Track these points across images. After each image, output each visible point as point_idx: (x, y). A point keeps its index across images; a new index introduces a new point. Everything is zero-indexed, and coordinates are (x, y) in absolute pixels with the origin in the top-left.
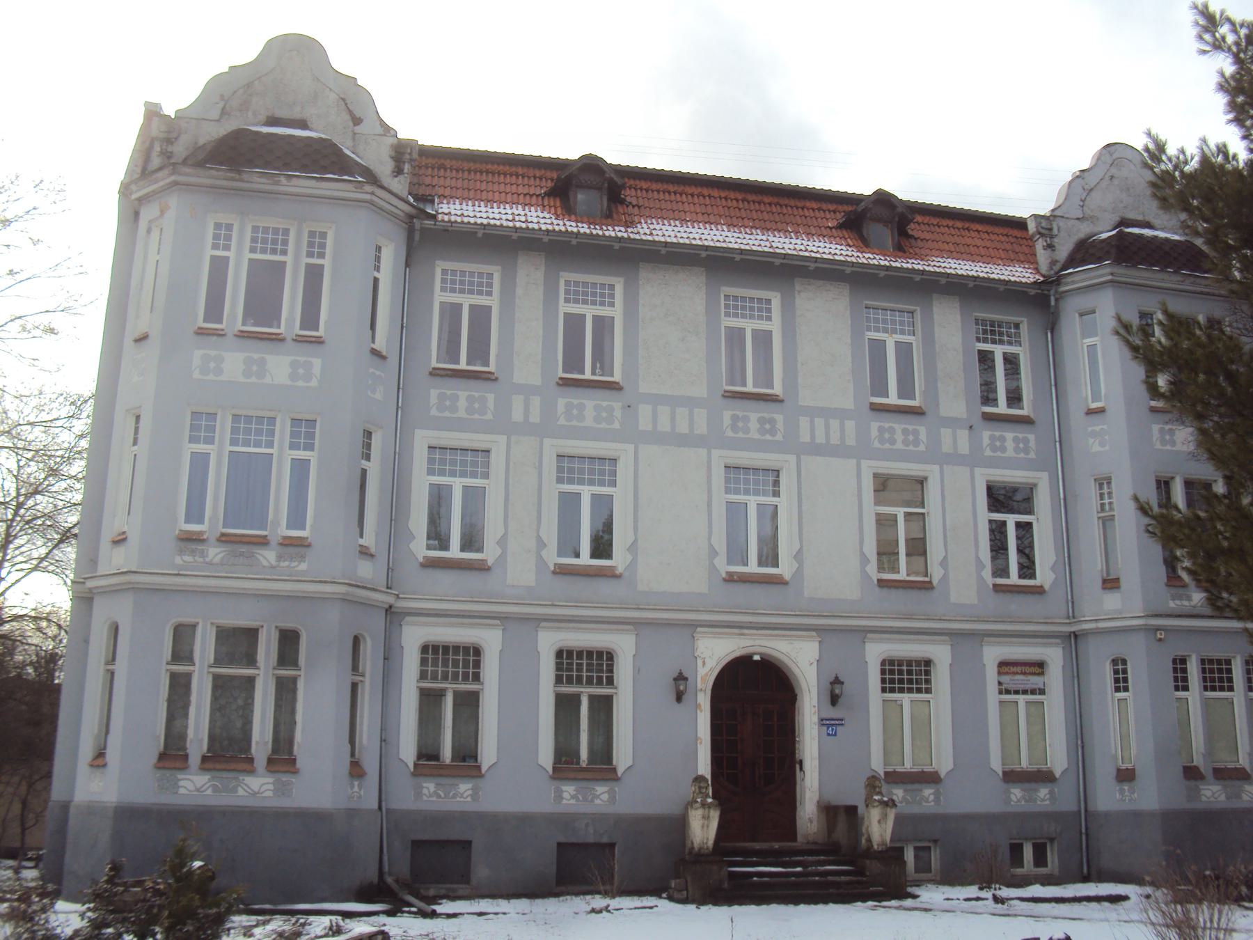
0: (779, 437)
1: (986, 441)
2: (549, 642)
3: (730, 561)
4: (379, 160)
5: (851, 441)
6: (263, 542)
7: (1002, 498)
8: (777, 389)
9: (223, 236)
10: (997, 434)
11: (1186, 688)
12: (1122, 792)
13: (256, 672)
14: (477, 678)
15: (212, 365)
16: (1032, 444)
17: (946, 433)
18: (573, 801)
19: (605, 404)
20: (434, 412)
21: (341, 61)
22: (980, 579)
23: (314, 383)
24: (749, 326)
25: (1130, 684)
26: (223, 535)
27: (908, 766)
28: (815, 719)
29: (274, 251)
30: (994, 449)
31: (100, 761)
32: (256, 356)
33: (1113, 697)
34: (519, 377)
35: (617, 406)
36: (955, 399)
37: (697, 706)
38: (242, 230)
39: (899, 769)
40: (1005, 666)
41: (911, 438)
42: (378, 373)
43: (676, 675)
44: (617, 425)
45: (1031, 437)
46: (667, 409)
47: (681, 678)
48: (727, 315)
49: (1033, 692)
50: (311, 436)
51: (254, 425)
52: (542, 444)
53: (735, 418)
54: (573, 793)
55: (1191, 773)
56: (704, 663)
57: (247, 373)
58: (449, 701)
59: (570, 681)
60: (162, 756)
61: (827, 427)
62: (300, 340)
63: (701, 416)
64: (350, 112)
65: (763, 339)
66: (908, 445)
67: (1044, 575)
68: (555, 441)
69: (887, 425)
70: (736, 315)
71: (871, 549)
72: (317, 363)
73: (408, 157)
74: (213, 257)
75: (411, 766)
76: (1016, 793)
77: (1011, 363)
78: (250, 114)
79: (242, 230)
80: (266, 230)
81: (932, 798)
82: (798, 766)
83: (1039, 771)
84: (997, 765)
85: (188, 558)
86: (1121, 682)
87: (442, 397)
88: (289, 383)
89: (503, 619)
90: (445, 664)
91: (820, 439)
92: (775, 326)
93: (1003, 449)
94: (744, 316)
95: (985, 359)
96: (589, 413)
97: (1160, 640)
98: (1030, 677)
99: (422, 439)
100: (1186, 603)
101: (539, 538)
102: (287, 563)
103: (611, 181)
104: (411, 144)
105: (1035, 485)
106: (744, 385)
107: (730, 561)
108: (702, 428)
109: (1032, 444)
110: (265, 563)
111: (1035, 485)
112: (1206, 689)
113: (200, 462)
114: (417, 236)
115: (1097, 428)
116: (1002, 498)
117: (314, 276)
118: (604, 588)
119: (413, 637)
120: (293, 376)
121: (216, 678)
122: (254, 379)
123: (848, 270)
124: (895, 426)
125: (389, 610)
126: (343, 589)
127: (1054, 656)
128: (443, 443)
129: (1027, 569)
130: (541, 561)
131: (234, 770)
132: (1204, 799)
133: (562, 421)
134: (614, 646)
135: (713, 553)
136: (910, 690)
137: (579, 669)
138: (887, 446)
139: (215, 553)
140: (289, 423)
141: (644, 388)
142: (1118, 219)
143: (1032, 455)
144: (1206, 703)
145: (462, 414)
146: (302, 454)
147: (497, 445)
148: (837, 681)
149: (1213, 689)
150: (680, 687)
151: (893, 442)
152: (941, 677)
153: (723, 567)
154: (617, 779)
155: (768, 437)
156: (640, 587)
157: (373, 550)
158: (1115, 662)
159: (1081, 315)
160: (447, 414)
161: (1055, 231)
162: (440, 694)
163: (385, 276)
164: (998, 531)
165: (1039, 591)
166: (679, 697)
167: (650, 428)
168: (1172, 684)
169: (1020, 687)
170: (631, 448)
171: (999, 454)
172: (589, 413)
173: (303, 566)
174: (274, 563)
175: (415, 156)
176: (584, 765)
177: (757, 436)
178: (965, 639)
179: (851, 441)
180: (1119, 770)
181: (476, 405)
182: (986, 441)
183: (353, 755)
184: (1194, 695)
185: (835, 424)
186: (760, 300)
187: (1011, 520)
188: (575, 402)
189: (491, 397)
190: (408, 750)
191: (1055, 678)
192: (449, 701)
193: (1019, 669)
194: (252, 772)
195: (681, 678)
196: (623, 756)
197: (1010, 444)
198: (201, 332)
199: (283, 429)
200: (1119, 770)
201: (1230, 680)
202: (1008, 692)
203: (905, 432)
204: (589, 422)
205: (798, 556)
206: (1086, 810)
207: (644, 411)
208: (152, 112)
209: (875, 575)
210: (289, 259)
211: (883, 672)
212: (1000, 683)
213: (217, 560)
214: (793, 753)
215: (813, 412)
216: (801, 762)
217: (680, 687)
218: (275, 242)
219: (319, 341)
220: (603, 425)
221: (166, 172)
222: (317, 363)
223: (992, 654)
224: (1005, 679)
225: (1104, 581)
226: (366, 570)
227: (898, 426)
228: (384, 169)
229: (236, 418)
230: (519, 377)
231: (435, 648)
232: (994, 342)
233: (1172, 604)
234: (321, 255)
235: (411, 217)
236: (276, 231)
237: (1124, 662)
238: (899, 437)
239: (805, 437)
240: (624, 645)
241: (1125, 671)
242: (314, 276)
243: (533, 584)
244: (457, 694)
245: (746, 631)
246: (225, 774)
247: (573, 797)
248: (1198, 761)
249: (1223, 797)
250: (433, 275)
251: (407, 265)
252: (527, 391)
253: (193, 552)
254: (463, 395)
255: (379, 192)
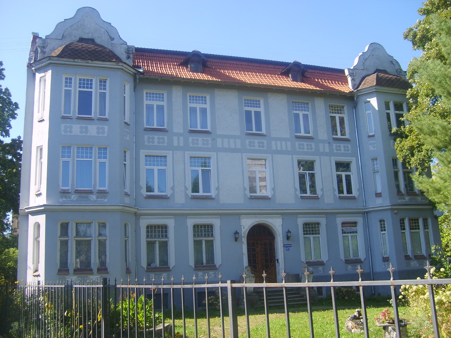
0: (265, 148)
1: (334, 147)
2: (191, 222)
3: (251, 192)
4: (121, 52)
5: (289, 149)
6: (91, 192)
7: (343, 166)
8: (209, 129)
9: (69, 81)
10: (338, 145)
11: (404, 229)
12: (385, 265)
13: (68, 238)
14: (166, 236)
15: (68, 129)
16: (350, 148)
17: (321, 145)
18: (202, 278)
19: (205, 138)
20: (146, 143)
21: (105, 17)
22: (334, 195)
23: (106, 135)
24: (198, 106)
25: (386, 228)
26: (76, 190)
27: (313, 260)
28: (282, 245)
29: (87, 88)
30: (337, 150)
31: (37, 274)
32: (84, 126)
33: (380, 233)
34: (175, 130)
35: (209, 139)
36: (323, 133)
37: (242, 242)
38: (76, 79)
39: (349, 258)
40: (344, 224)
41: (309, 147)
42: (127, 130)
43: (235, 232)
44: (210, 146)
45: (349, 146)
46: (176, 137)
47: (236, 233)
48: (190, 102)
49: (353, 232)
50: (105, 154)
51: (85, 149)
52: (330, 158)
53: (250, 142)
54: (202, 275)
55: (407, 257)
56: (244, 228)
57: (81, 132)
58: (157, 245)
59: (198, 236)
60: (59, 271)
61: (281, 144)
62: (99, 119)
63: (238, 142)
64: (110, 36)
65: (204, 111)
66: (308, 150)
67: (355, 193)
68: (189, 152)
69: (301, 143)
70: (248, 106)
71: (247, 186)
72: (106, 128)
73: (131, 52)
74: (79, 91)
75: (146, 269)
76: (350, 267)
77: (342, 121)
78: (73, 37)
79: (76, 79)
80: (84, 80)
81: (322, 270)
82: (276, 262)
83: (357, 259)
84: (342, 257)
85: (65, 199)
86: (383, 229)
87: (149, 138)
88: (97, 135)
89: (175, 215)
90: (155, 232)
91: (279, 148)
92: (207, 106)
93: (340, 150)
94: (153, 100)
95: (333, 118)
96: (200, 142)
97: (396, 213)
98: (352, 228)
99: (143, 153)
100: (403, 200)
101: (185, 186)
102: (100, 199)
103: (203, 59)
104: (132, 47)
105: (315, 161)
106: (153, 125)
107: (251, 192)
108: (239, 146)
109: (350, 148)
110: (92, 200)
111: (315, 161)
112: (411, 229)
113: (66, 164)
114: (138, 80)
115: (372, 142)
116: (343, 166)
117: (103, 96)
118: (209, 203)
119: (144, 223)
120: (98, 133)
121: (77, 241)
122: (84, 134)
123: (287, 90)
124: (304, 143)
125: (135, 214)
126: (120, 208)
127: (360, 220)
128: (194, 155)
129: (349, 191)
130: (186, 195)
131: (86, 274)
132: (412, 266)
133: (191, 145)
134: (213, 223)
135: (186, 189)
136: (313, 234)
137: (201, 232)
138: (302, 150)
139: (74, 197)
140: (97, 149)
141: (219, 132)
142: (375, 69)
143: (350, 152)
144: (411, 233)
145: (156, 144)
146: (102, 160)
147: (169, 154)
148: (289, 232)
149: (413, 229)
150: (236, 236)
151: (303, 149)
152: (323, 229)
153: (249, 194)
154: (217, 269)
155: (262, 148)
156: (221, 202)
157: (129, 193)
158: (380, 221)
159: (365, 103)
160: (151, 144)
161: (355, 74)
162: (154, 243)
163: (127, 95)
164: (302, 177)
165: (354, 198)
166: (236, 239)
167: (221, 146)
168: (400, 228)
169: (349, 231)
170: (215, 154)
171: (339, 152)
172: (200, 142)
173: (106, 200)
174: (96, 200)
175: (134, 52)
176: (158, 266)
177: (258, 148)
178: (330, 215)
179: (289, 149)
180: (383, 258)
181: (161, 140)
182: (334, 147)
183: (126, 266)
184: (407, 231)
185: (284, 143)
186: (159, 94)
187: (344, 174)
188: (195, 138)
189: (166, 138)
190: (144, 264)
191: (360, 228)
192: (157, 245)
193: (348, 225)
194: (92, 274)
195: (236, 233)
196: (218, 260)
197: (342, 148)
198: (63, 118)
199: (95, 151)
200: (383, 258)
201: (418, 226)
202: (345, 233)
203: (307, 145)
204: (200, 145)
205: (218, 189)
206: (373, 272)
207: (219, 141)
208: (36, 37)
209: (300, 195)
210: (93, 90)
211: (304, 228)
212: (342, 230)
213: (75, 199)
214: (274, 257)
215: (276, 139)
216: (278, 260)
217: (236, 236)
218: (87, 84)
219: (106, 120)
220: (205, 146)
221: (47, 59)
222: (106, 128)
223: (339, 220)
224: (344, 228)
225: (376, 194)
226: (127, 200)
227: (305, 143)
228: (123, 57)
229: (78, 148)
230: (175, 130)
231: (151, 226)
232: (335, 113)
233: (399, 201)
234: (105, 89)
235: (135, 74)
236: (88, 80)
237: (384, 221)
238: (305, 147)
239: (274, 148)
240: (216, 222)
241: (384, 224)
242: (103, 96)
243: (184, 203)
244: (160, 242)
245: (257, 216)
246: (83, 275)
247: (202, 276)
248: (409, 253)
249: (418, 265)
250: (143, 94)
251: (134, 91)
252: (179, 135)
253: (66, 197)
254: (156, 137)
255: (125, 65)
